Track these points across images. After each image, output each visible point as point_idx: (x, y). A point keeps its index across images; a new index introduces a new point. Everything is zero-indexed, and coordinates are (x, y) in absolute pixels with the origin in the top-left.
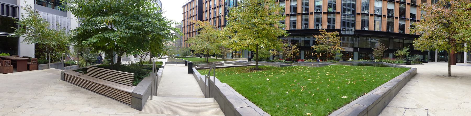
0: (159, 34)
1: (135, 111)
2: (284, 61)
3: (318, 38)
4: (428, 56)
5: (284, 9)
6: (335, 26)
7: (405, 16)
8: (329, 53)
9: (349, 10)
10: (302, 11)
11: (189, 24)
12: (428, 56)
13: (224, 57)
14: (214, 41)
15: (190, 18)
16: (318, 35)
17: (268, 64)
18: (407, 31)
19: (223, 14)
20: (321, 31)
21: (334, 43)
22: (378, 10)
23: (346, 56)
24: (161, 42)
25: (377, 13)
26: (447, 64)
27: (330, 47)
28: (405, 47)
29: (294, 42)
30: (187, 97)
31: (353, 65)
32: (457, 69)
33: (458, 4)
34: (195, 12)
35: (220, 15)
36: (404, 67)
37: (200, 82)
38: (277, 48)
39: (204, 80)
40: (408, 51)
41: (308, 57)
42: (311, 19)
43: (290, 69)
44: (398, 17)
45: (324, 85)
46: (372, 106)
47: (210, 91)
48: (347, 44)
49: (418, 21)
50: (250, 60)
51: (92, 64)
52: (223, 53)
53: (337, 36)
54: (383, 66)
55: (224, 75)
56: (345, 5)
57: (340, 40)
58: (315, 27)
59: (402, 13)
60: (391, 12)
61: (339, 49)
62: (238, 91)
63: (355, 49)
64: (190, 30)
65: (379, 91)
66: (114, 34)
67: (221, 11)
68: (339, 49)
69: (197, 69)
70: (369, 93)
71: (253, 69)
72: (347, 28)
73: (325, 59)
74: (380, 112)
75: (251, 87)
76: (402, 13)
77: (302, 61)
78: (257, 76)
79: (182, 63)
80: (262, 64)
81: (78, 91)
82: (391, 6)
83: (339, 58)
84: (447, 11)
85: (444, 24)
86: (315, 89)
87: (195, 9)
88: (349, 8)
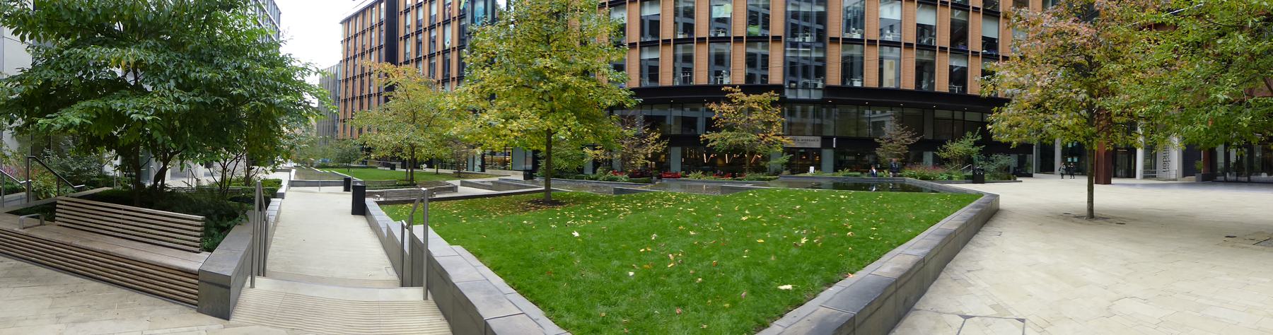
0: (272, 105)
1: (214, 324)
2: (624, 177)
3: (720, 110)
4: (1030, 159)
5: (622, 28)
6: (766, 77)
7: (966, 45)
8: (752, 154)
9: (806, 29)
10: (675, 33)
11: (358, 72)
12: (1034, 158)
13: (458, 168)
14: (430, 122)
15: (363, 54)
16: (718, 102)
17: (579, 187)
18: (975, 86)
19: (456, 45)
20: (727, 92)
21: (765, 124)
22: (891, 28)
23: (799, 161)
24: (275, 124)
25: (889, 37)
26: (1082, 182)
27: (755, 138)
28: (969, 134)
29: (654, 123)
30: (345, 282)
31: (819, 186)
32: (1112, 195)
33: (1117, 9)
34: (376, 38)
35: (447, 46)
36: (964, 192)
37: (387, 242)
38: (604, 141)
39: (398, 235)
40: (977, 144)
41: (691, 165)
42: (701, 56)
43: (642, 200)
44: (948, 46)
45: (734, 251)
46: (868, 312)
47: (415, 268)
48: (804, 125)
49: (1005, 58)
50: (529, 175)
51: (80, 190)
52: (458, 156)
53: (774, 104)
54: (906, 188)
55: (457, 220)
56: (795, 15)
57: (782, 114)
58: (712, 79)
59: (959, 34)
60: (927, 32)
61: (780, 141)
62: (496, 269)
63: (826, 141)
64: (362, 89)
65: (890, 265)
66: (142, 102)
67: (450, 36)
68: (780, 141)
69: (379, 203)
70: (861, 274)
71: (537, 202)
72: (801, 81)
73: (742, 172)
74: (893, 326)
75: (528, 256)
76: (959, 34)
77: (676, 176)
78: (547, 222)
79: (336, 184)
80: (563, 188)
81: (24, 279)
82: (927, 17)
83: (779, 167)
84: (1084, 29)
85: (1078, 67)
86: (706, 263)
87: (376, 30)
88: (807, 25)
